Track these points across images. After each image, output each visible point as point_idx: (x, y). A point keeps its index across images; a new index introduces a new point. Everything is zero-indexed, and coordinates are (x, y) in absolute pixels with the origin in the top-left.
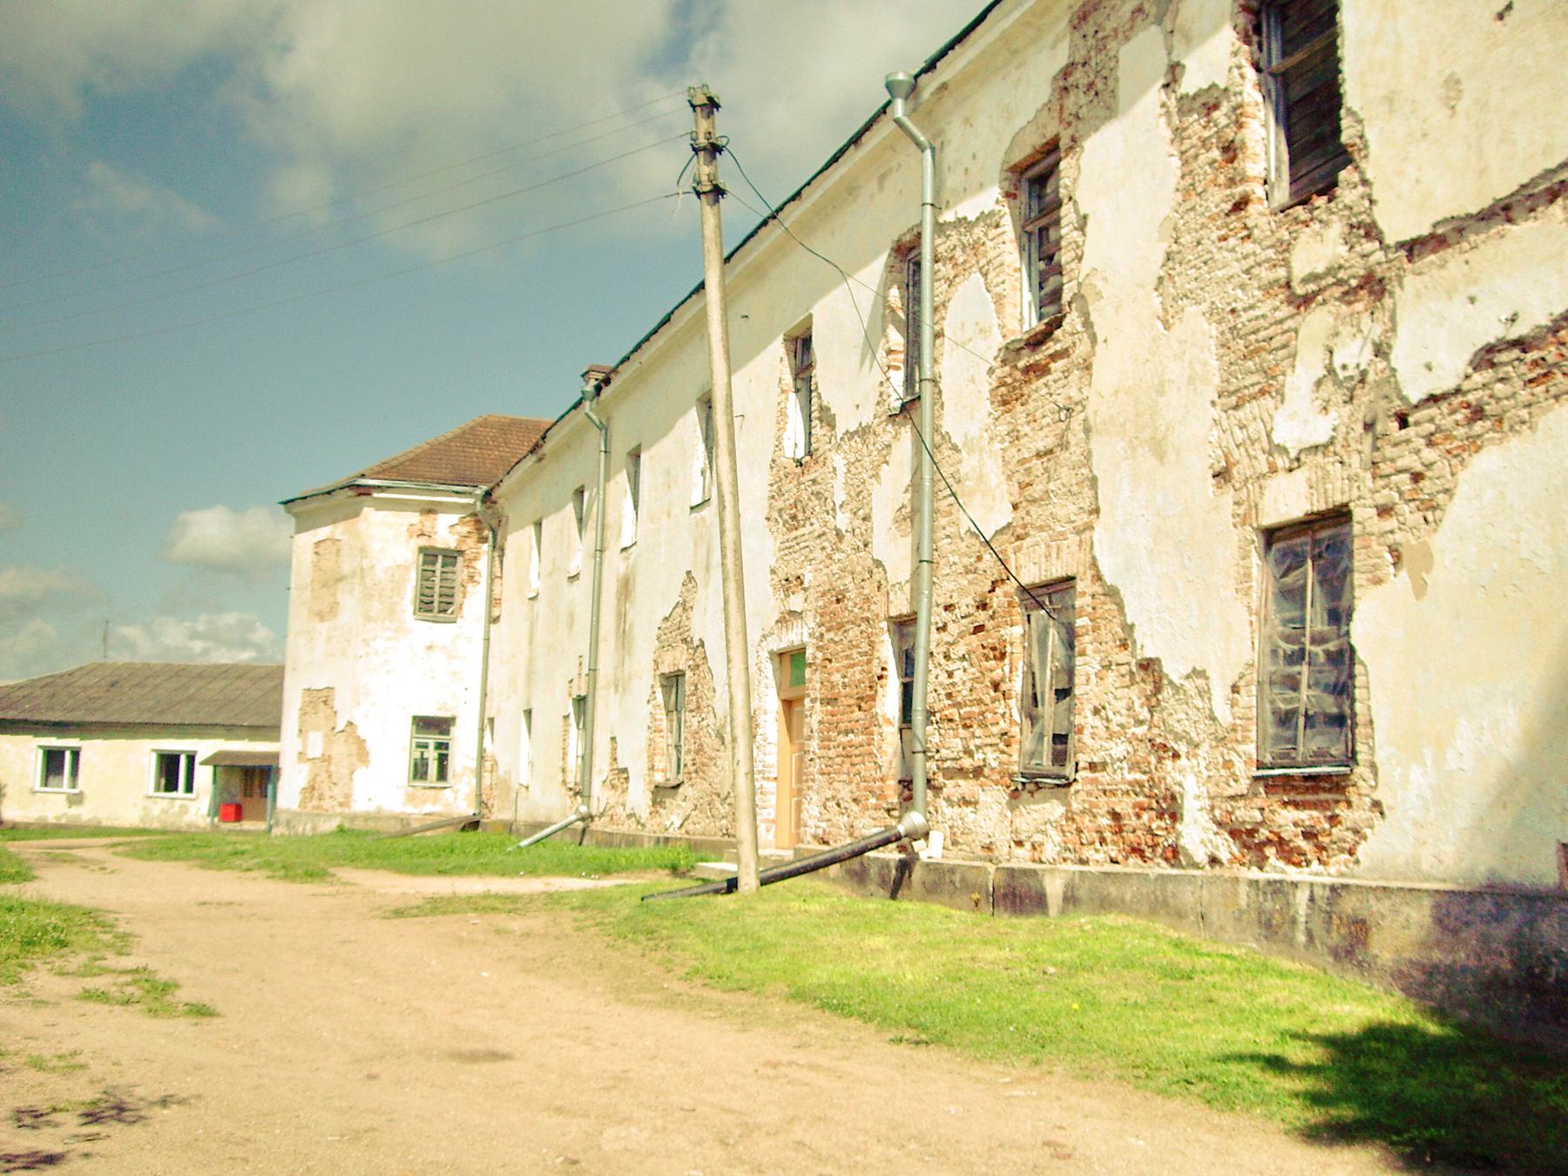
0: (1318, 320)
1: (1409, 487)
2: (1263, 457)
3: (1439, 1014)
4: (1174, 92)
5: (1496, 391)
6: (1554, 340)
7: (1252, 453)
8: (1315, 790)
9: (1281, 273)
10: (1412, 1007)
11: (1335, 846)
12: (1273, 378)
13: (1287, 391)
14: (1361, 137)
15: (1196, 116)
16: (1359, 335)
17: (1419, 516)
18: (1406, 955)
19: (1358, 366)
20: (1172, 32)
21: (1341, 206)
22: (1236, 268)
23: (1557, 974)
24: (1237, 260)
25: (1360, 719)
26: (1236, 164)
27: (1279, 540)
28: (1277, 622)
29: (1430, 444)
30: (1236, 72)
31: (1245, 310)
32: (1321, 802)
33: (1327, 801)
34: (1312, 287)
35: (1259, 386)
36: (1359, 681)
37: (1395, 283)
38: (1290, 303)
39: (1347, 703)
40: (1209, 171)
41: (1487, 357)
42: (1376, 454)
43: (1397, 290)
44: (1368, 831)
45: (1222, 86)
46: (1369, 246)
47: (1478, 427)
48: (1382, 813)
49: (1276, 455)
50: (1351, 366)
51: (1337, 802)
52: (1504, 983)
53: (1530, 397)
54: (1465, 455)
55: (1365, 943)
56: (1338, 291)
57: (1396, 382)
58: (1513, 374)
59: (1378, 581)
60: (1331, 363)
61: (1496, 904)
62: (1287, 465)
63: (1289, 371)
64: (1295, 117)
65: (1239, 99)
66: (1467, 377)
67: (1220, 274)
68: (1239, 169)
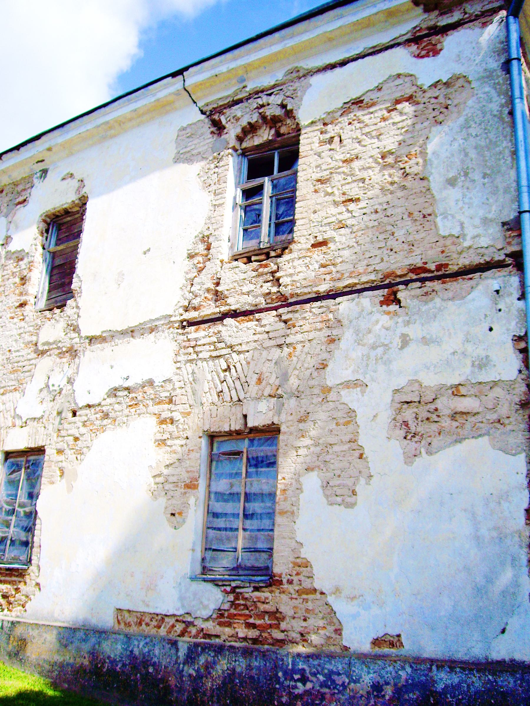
0: (46, 362)
1: (72, 443)
2: (10, 419)
3: (54, 685)
4: (5, 248)
5: (115, 408)
6: (141, 390)
7: (6, 416)
8: (11, 575)
9: (34, 339)
10: (42, 682)
11: (16, 603)
12: (22, 384)
13: (26, 391)
14: (80, 288)
15: (12, 261)
16: (62, 372)
17: (74, 456)
18: (43, 657)
19: (59, 386)
20: (11, 222)
21: (65, 315)
22: (15, 332)
23: (108, 667)
24: (16, 329)
25: (35, 545)
26: (24, 286)
27: (11, 457)
28: (4, 495)
29: (84, 425)
30: (34, 247)
31: (15, 351)
32: (13, 581)
33: (15, 581)
34: (46, 347)
35: (14, 387)
36: (37, 527)
37: (82, 353)
38: (35, 353)
39: (31, 536)
40: (12, 287)
41: (114, 392)
42: (60, 426)
43: (82, 356)
44: (32, 597)
45: (26, 252)
46: (74, 335)
47: (105, 422)
48: (40, 589)
49: (16, 419)
50: (56, 385)
51: (20, 582)
52: (85, 671)
53: (128, 413)
54: (98, 433)
55: (24, 650)
56: (58, 351)
57: (74, 397)
58: (123, 402)
59: (53, 483)
60: (48, 382)
61: (85, 634)
62: (21, 424)
63: (29, 383)
64: (55, 272)
65: (32, 259)
66: (105, 399)
67: (7, 333)
68: (25, 289)
